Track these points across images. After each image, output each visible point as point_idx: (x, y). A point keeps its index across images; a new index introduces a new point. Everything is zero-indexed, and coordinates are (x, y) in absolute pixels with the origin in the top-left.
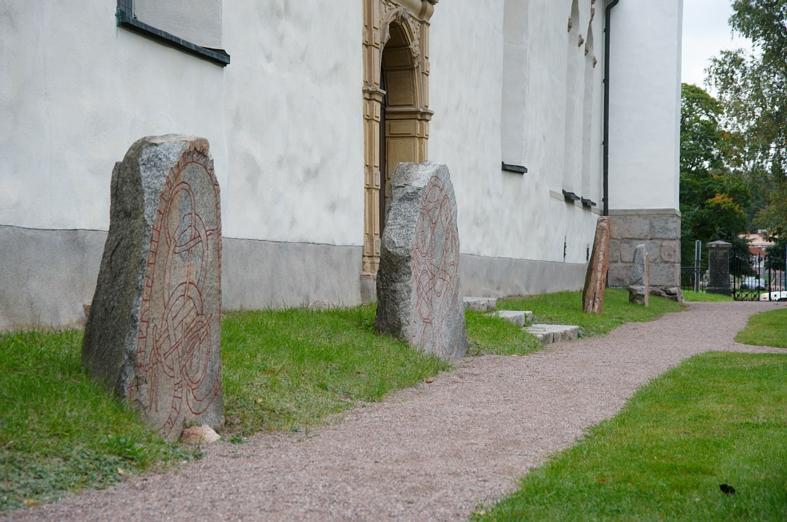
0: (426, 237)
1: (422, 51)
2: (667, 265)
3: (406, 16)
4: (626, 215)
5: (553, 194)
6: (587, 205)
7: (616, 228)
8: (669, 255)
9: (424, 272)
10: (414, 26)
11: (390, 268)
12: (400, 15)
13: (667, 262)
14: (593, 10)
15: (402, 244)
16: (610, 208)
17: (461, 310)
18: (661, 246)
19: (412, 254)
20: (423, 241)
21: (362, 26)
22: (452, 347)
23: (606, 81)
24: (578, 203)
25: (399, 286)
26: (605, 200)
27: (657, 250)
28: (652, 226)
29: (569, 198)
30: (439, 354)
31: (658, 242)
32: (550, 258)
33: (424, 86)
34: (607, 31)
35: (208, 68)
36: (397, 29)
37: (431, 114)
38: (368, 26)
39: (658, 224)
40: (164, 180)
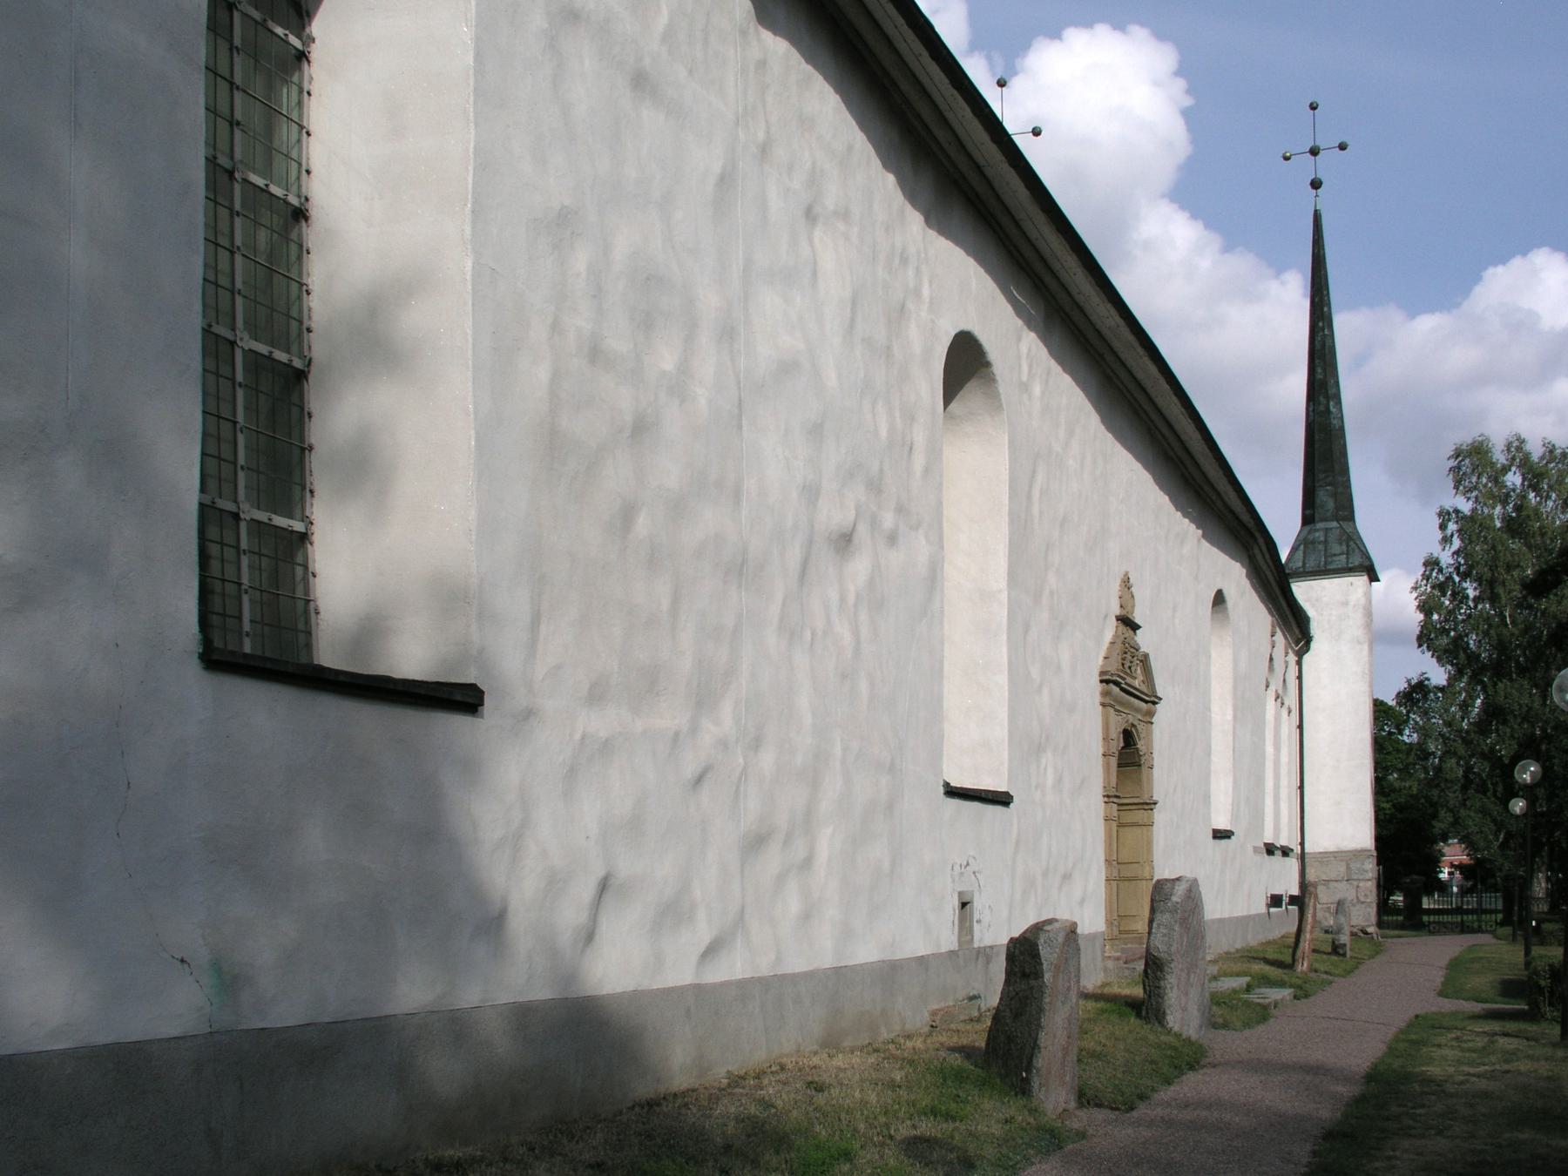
0: (1183, 941)
1: (1148, 749)
2: (1363, 906)
3: (1136, 723)
4: (1326, 857)
5: (1256, 849)
6: (1286, 852)
7: (1313, 871)
8: (1366, 895)
9: (1182, 970)
10: (1141, 727)
11: (1154, 967)
12: (1130, 722)
13: (1363, 903)
14: (1286, 662)
15: (1166, 950)
16: (1306, 851)
17: (1207, 995)
18: (1358, 887)
19: (1174, 958)
20: (1182, 945)
21: (1101, 739)
22: (1201, 1027)
23: (1300, 727)
24: (1278, 853)
25: (1162, 983)
26: (1302, 844)
27: (1354, 891)
28: (1348, 868)
29: (1270, 849)
30: (1104, 980)
31: (1355, 883)
32: (1253, 912)
33: (1150, 779)
34: (1300, 678)
35: (998, 809)
36: (1128, 737)
37: (1155, 804)
38: (1106, 739)
39: (1354, 866)
40: (1056, 955)
